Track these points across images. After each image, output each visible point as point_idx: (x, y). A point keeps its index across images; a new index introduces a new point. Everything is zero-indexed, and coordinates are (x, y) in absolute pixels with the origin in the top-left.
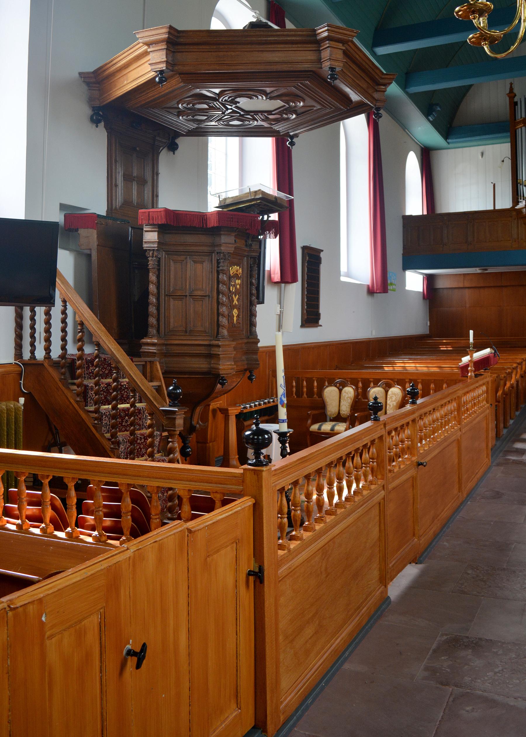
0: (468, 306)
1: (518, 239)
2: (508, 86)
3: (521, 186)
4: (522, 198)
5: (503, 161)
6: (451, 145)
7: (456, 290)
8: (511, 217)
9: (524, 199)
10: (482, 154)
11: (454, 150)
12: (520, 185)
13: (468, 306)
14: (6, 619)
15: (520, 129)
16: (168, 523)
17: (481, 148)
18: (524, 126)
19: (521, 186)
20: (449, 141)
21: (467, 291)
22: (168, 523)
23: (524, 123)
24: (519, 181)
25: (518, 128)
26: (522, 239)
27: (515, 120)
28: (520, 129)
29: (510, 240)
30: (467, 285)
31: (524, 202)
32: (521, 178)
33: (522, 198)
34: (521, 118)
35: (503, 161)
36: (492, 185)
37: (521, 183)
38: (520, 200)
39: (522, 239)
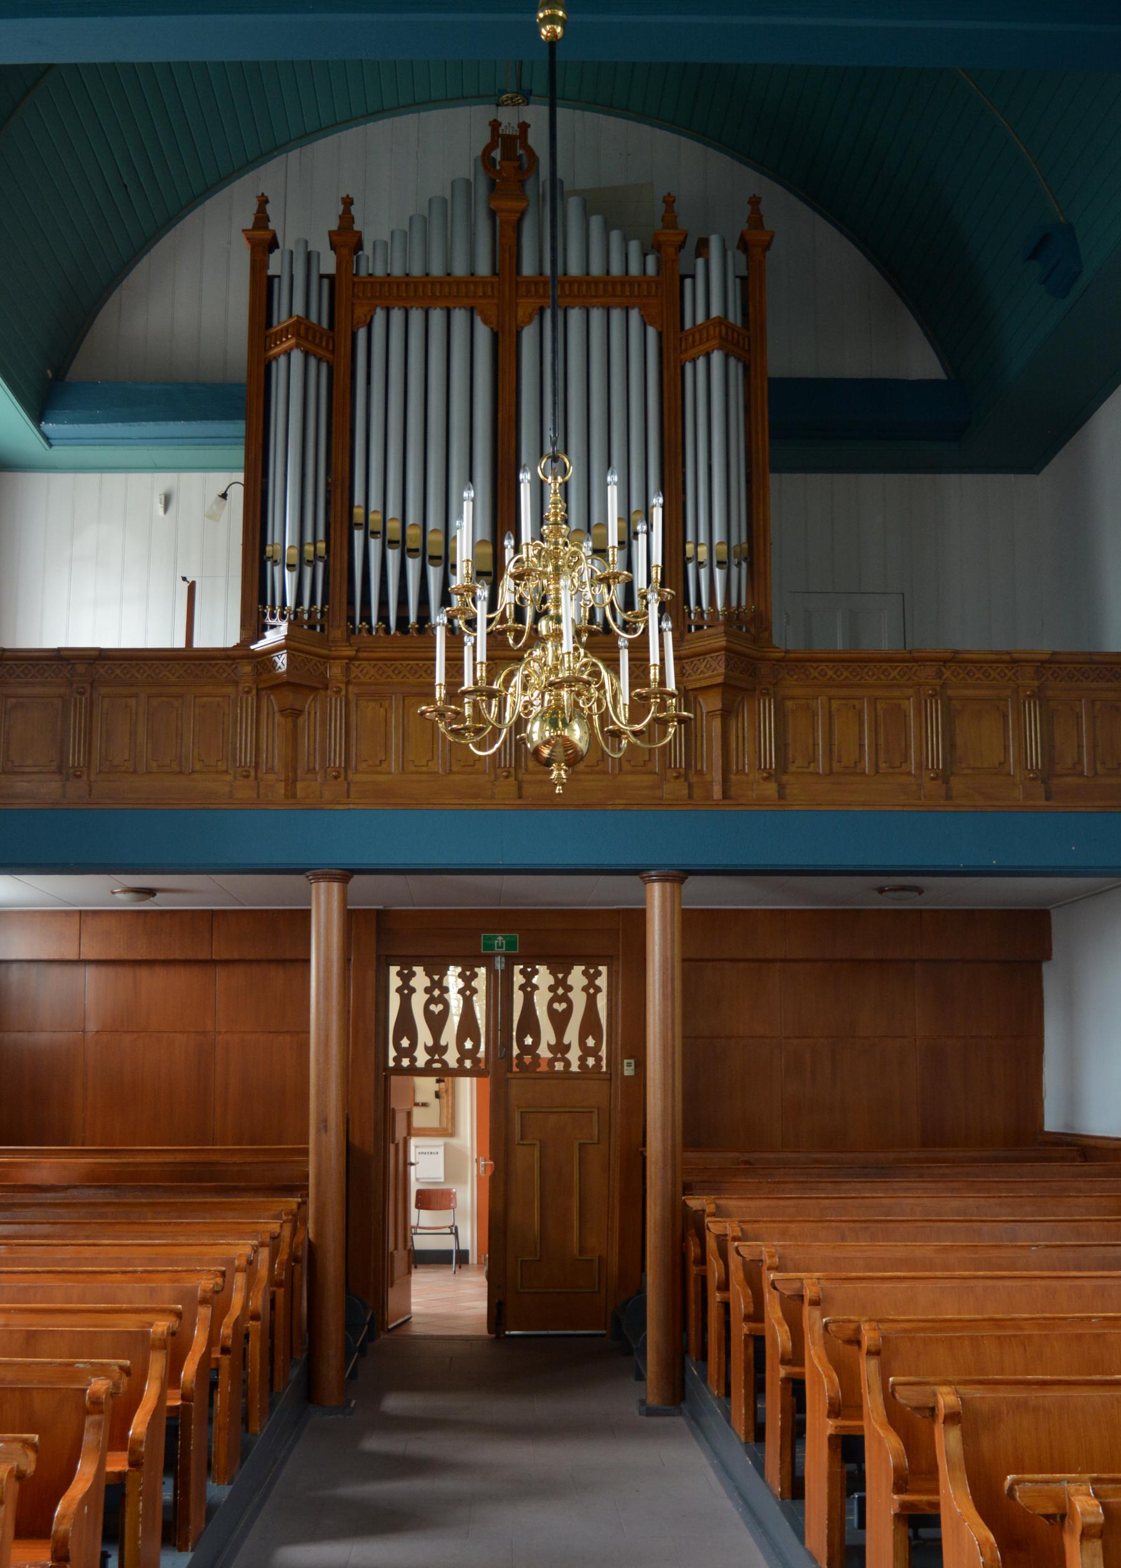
0: (92, 1027)
1: (257, 766)
2: (254, 206)
3: (277, 569)
4: (278, 611)
5: (224, 496)
6: (59, 453)
7: (56, 971)
8: (236, 683)
9: (283, 617)
10: (167, 501)
11: (69, 477)
12: (275, 563)
13: (92, 1027)
14: (931, 1379)
15: (283, 360)
16: (760, 1467)
17: (164, 481)
18: (297, 346)
19: (277, 569)
20: (49, 427)
21: (90, 972)
22: (760, 1467)
23: (297, 335)
24: (269, 549)
25: (276, 358)
26: (271, 770)
27: (269, 324)
28: (283, 360)
29: (226, 772)
30: (90, 952)
31: (284, 627)
32: (277, 539)
33: (278, 611)
34: (290, 315)
35: (224, 496)
36: (186, 585)
37: (278, 557)
38: (269, 621)
39: (271, 770)
